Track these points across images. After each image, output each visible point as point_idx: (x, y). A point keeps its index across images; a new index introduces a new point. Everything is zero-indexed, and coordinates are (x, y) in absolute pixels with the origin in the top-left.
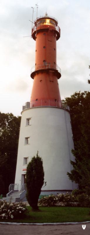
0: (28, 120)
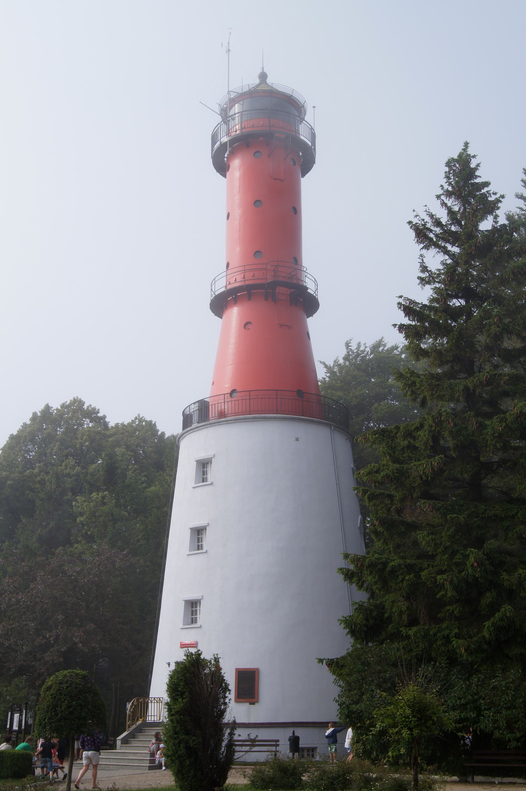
0: (198, 533)
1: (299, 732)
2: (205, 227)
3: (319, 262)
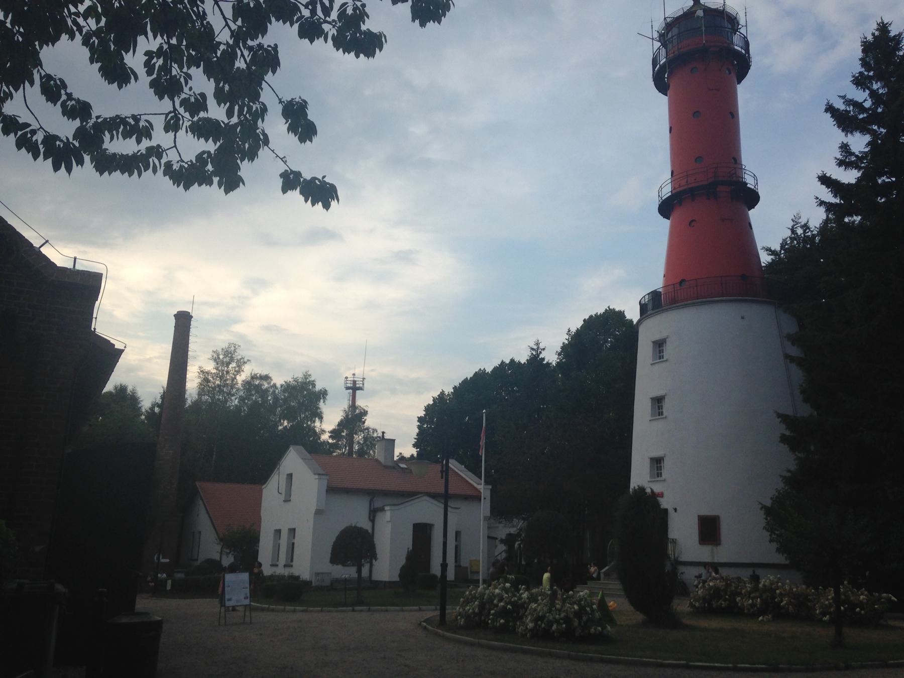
0: (658, 402)
1: (759, 572)
2: (642, 141)
3: (756, 160)
